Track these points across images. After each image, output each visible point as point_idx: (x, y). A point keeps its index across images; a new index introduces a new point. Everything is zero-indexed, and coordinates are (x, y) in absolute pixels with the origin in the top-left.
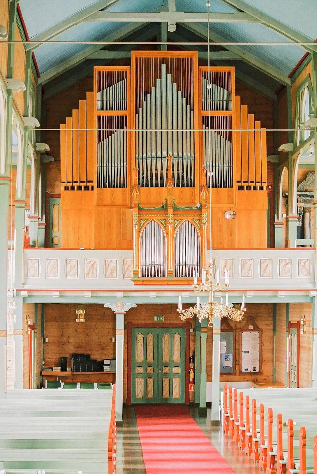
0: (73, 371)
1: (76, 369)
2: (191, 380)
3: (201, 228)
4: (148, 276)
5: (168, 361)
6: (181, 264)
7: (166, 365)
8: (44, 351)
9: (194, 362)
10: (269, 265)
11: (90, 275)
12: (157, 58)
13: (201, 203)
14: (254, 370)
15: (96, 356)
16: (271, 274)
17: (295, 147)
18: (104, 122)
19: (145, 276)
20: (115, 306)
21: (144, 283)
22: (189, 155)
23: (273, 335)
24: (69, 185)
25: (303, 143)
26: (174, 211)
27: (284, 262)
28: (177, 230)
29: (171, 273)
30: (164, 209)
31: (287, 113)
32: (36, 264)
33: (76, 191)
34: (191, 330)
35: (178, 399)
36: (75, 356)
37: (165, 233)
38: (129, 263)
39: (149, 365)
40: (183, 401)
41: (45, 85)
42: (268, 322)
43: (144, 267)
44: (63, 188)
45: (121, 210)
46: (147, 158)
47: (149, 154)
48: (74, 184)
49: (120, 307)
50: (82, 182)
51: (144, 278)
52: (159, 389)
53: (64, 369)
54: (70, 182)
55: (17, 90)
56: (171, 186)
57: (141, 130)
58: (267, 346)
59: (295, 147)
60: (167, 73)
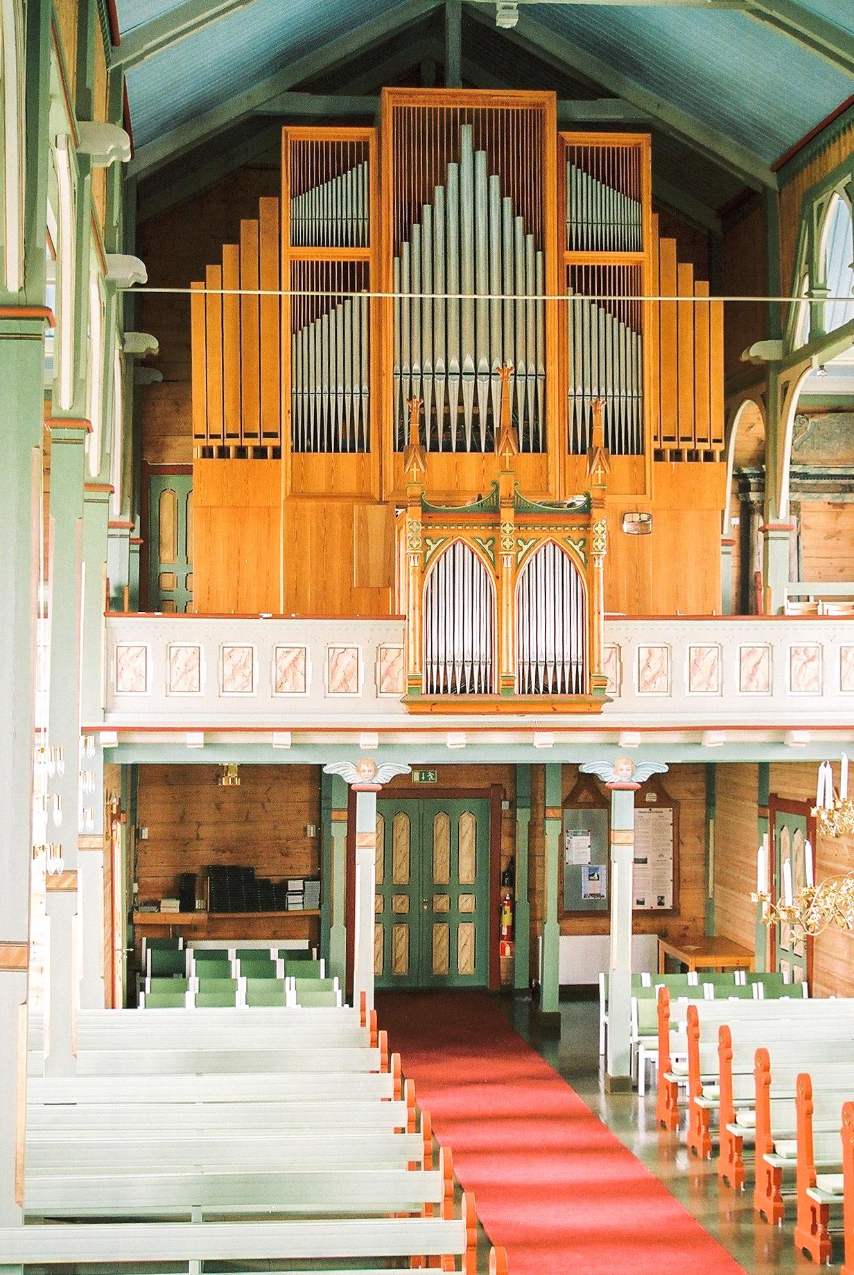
0: (211, 911)
1: (217, 905)
2: (505, 932)
3: (588, 562)
4: (441, 691)
7: (441, 890)
8: (136, 860)
10: (764, 662)
11: (287, 687)
12: (449, 110)
13: (587, 495)
14: (660, 903)
15: (268, 870)
16: (769, 687)
17: (787, 350)
18: (306, 274)
19: (438, 691)
22: (531, 369)
25: (819, 341)
26: (517, 513)
29: (509, 680)
33: (233, 462)
34: (505, 805)
36: (216, 872)
37: (491, 577)
38: (394, 653)
39: (400, 890)
40: (483, 983)
42: (693, 786)
43: (435, 667)
44: (197, 452)
45: (356, 507)
47: (428, 364)
49: (364, 771)
50: (248, 435)
51: (434, 697)
53: (187, 907)
54: (218, 437)
55: (107, 157)
59: (787, 350)
60: (475, 148)
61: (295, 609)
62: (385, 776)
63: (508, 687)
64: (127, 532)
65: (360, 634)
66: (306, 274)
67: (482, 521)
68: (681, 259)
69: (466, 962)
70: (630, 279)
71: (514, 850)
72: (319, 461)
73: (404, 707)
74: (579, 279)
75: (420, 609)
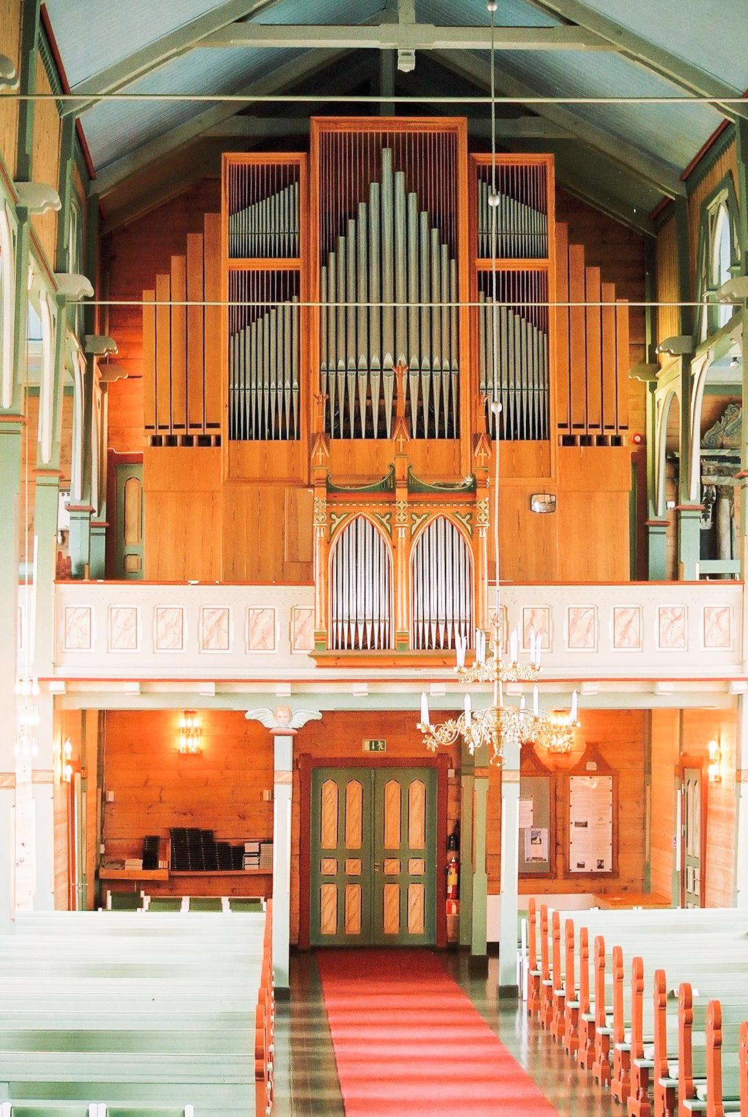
0: (173, 869)
1: (179, 863)
2: (450, 890)
10: (635, 620)
11: (212, 644)
14: (600, 867)
15: (226, 833)
16: (639, 643)
18: (243, 284)
19: (343, 647)
22: (446, 364)
24: (164, 433)
26: (410, 492)
27: (670, 615)
28: (418, 537)
29: (402, 639)
32: (86, 620)
33: (179, 449)
37: (389, 547)
38: (306, 614)
40: (433, 942)
43: (353, 627)
45: (287, 490)
47: (352, 361)
50: (192, 426)
51: (340, 652)
53: (150, 863)
54: (166, 427)
60: (395, 169)
61: (232, 578)
62: (299, 721)
63: (402, 639)
64: (87, 515)
65: (274, 600)
66: (243, 284)
67: (381, 499)
68: (589, 263)
69: (416, 924)
70: (532, 285)
71: (459, 814)
72: (254, 447)
73: (314, 662)
74: (483, 282)
75: (326, 575)
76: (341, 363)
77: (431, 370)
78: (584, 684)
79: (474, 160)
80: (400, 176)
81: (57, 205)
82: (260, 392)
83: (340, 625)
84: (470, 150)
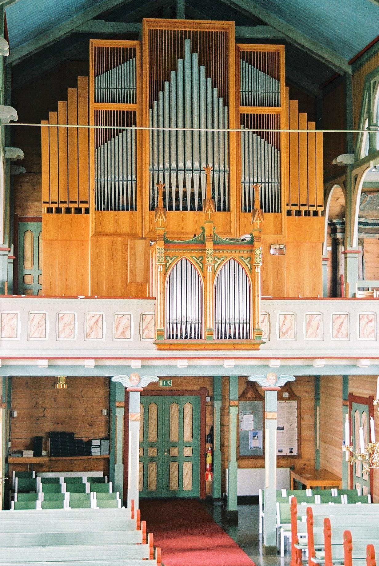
0: (51, 456)
1: (54, 453)
2: (208, 466)
4: (174, 338)
5: (176, 439)
6: (223, 321)
7: (174, 445)
9: (212, 442)
11: (92, 335)
14: (291, 452)
15: (82, 434)
16: (348, 335)
17: (357, 158)
19: (173, 338)
20: (128, 380)
21: (171, 347)
22: (222, 167)
23: (316, 405)
24: (54, 206)
28: (219, 272)
29: (210, 333)
30: (200, 243)
31: (345, 114)
32: (14, 321)
33: (64, 215)
35: (189, 491)
36: (53, 435)
38: (149, 318)
40: (196, 494)
41: (16, 66)
42: (307, 388)
44: (44, 210)
45: (129, 241)
46: (158, 170)
47: (167, 165)
48: (61, 205)
49: (133, 381)
50: (71, 202)
52: (164, 477)
53: (37, 454)
54: (56, 203)
56: (211, 210)
57: (173, 129)
58: (307, 420)
60: (192, 52)
62: (144, 384)
63: (210, 333)
68: (301, 110)
69: (187, 484)
70: (275, 121)
71: (213, 422)
72: (109, 215)
73: (155, 346)
76: (161, 166)
77: (127, 180)
78: (316, 360)
79: (238, 47)
80: (196, 56)
81: (6, 51)
82: (113, 182)
83: (171, 325)
84: (236, 42)
